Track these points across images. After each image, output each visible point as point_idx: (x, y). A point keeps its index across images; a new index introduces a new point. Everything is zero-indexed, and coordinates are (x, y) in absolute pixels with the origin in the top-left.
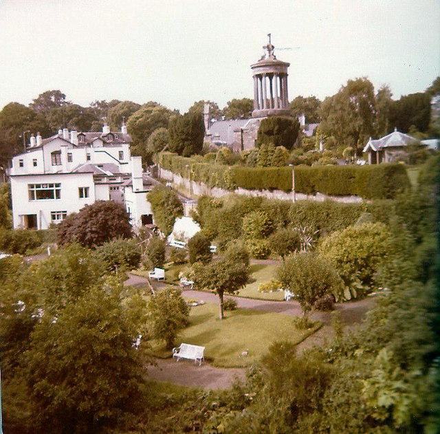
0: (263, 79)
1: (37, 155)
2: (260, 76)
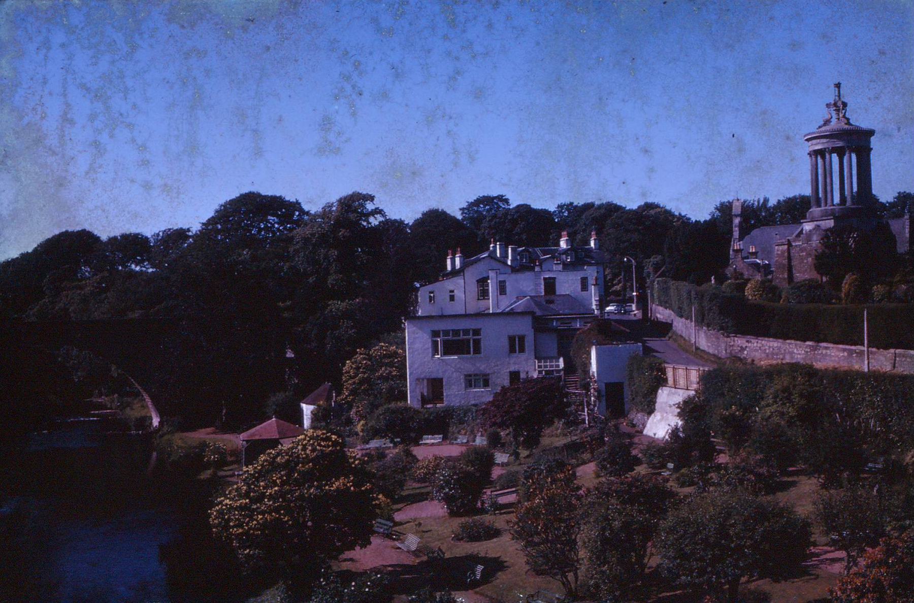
0: (827, 156)
1: (457, 285)
2: (820, 153)
